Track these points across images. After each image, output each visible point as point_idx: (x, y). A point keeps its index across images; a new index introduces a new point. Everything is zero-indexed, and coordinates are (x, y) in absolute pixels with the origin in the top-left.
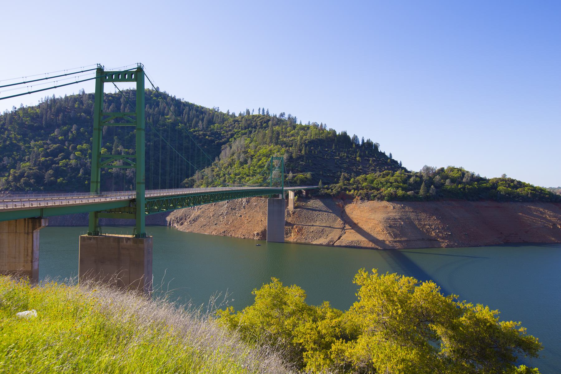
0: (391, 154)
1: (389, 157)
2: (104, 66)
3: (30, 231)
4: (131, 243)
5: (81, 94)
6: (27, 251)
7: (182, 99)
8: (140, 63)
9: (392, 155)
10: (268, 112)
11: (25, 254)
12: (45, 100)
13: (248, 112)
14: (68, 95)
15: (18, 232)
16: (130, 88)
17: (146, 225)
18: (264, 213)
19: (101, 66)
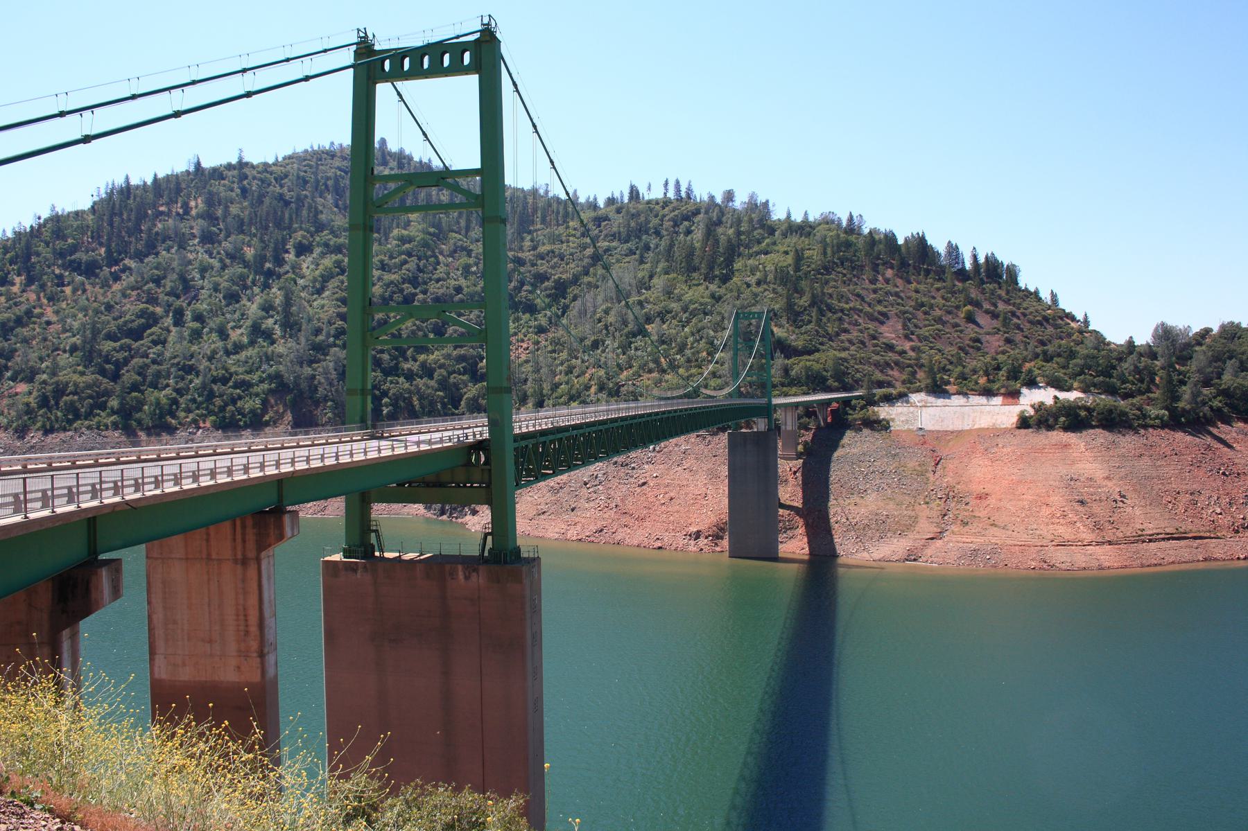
0: (1054, 296)
2: (374, 36)
3: (251, 554)
4: (481, 581)
5: (192, 169)
6: (246, 620)
8: (490, 16)
9: (1059, 297)
11: (238, 630)
12: (106, 193)
13: (634, 193)
14: (161, 175)
15: (214, 556)
16: (312, 147)
18: (713, 475)
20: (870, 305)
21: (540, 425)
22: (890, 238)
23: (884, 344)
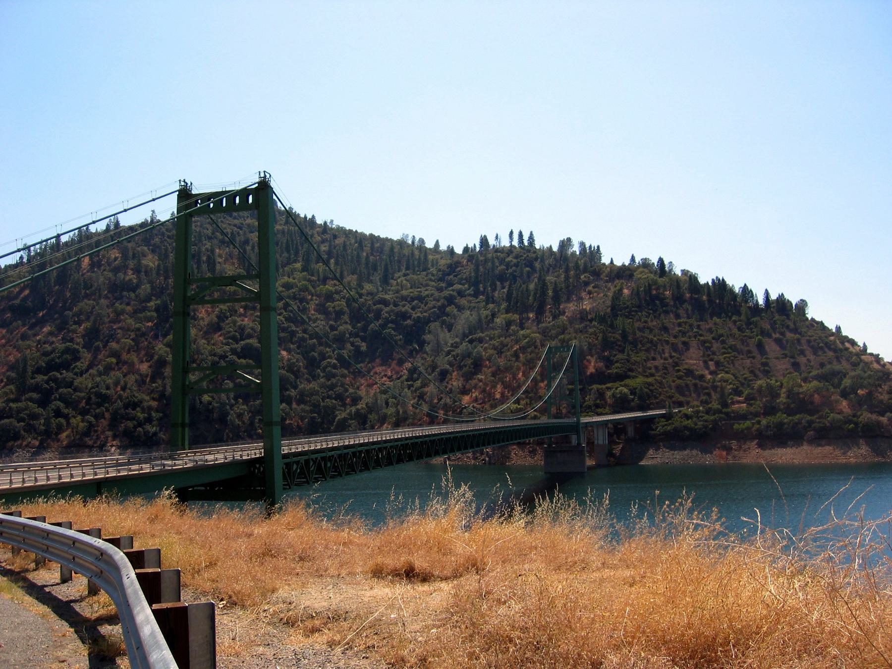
1: (834, 331)
2: (191, 184)
7: (328, 221)
8: (264, 172)
10: (531, 238)
13: (484, 241)
17: (132, 548)
19: (187, 184)
20: (675, 337)
21: (416, 434)
22: (692, 279)
23: (685, 369)
